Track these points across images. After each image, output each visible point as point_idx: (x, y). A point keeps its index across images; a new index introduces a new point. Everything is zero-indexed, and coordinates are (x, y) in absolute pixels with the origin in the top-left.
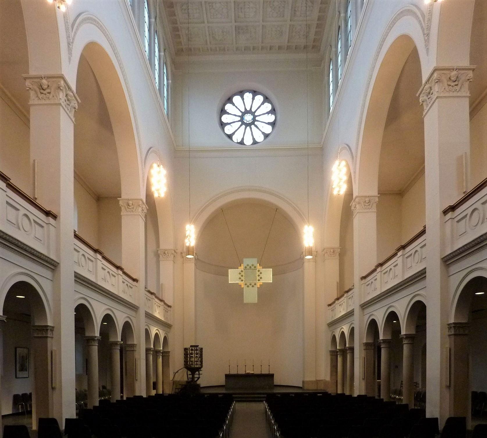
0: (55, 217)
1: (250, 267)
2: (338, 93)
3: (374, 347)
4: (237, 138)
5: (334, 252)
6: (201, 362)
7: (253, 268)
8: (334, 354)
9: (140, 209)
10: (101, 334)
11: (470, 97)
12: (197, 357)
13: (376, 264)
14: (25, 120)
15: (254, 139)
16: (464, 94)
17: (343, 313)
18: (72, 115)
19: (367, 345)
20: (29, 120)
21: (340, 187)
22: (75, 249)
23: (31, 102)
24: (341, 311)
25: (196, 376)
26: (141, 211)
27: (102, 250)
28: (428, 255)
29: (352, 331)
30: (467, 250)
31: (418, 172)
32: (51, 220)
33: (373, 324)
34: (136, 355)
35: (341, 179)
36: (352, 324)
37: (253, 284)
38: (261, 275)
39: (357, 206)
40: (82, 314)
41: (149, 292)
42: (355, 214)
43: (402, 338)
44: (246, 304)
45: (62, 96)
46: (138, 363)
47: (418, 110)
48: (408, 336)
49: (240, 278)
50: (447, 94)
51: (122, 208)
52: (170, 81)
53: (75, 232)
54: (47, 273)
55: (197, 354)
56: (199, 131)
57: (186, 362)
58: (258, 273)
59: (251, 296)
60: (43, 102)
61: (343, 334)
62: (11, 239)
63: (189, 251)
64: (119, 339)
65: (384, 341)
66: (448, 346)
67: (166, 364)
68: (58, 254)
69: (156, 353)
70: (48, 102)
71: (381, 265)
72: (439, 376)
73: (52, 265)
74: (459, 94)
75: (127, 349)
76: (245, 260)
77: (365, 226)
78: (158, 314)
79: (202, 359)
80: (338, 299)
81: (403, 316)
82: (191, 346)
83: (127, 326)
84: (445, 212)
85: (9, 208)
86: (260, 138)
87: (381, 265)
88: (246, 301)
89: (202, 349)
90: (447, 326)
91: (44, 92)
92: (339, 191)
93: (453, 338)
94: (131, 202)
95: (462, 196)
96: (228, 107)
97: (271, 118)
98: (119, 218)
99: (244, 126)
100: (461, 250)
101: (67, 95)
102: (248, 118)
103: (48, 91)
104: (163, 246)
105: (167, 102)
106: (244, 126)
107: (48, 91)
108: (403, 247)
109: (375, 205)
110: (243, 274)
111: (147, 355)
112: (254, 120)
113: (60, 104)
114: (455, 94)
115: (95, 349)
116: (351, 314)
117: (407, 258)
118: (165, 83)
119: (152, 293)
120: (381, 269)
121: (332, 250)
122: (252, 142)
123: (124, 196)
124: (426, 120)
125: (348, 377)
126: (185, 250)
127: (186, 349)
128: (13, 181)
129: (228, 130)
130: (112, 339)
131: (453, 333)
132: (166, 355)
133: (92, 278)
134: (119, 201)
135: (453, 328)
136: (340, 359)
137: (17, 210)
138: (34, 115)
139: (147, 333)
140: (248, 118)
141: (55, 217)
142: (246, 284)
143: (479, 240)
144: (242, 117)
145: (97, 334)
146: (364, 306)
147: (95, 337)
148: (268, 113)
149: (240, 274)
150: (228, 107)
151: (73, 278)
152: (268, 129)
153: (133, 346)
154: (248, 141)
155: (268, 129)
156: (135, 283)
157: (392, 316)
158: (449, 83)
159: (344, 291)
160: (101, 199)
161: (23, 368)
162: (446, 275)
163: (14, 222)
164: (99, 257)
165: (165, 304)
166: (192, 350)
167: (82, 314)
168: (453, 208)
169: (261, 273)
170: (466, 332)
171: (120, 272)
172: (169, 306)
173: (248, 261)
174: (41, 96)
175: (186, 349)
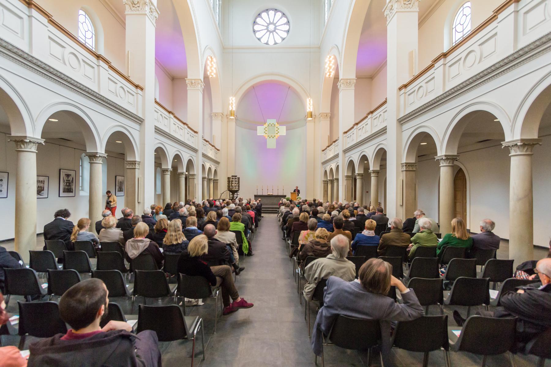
2: (331, 8)
4: (264, 40)
6: (239, 186)
8: (326, 183)
9: (200, 86)
10: (172, 167)
11: (419, 13)
13: (353, 123)
14: (122, 23)
15: (275, 41)
16: (415, 10)
17: (332, 156)
18: (154, 22)
20: (125, 24)
21: (330, 72)
22: (155, 111)
23: (126, 13)
24: (330, 154)
25: (235, 196)
26: (200, 87)
27: (172, 111)
28: (388, 117)
29: (338, 167)
30: (410, 117)
31: (382, 65)
32: (139, 91)
33: (351, 163)
35: (330, 67)
41: (205, 140)
43: (370, 173)
44: (269, 149)
45: (147, 9)
46: (197, 185)
47: (383, 20)
48: (374, 172)
50: (403, 10)
51: (188, 85)
52: (221, 2)
53: (155, 99)
54: (137, 126)
56: (240, 34)
57: (229, 186)
58: (276, 129)
59: (271, 144)
60: (135, 13)
61: (331, 169)
63: (231, 113)
64: (185, 171)
65: (359, 175)
66: (401, 178)
68: (144, 113)
69: (209, 180)
70: (137, 12)
71: (357, 124)
73: (139, 121)
74: (412, 10)
77: (347, 99)
78: (211, 153)
80: (328, 147)
81: (441, 137)
83: (190, 163)
84: (400, 89)
85: (110, 81)
86: (279, 40)
87: (357, 124)
88: (268, 147)
91: (136, 6)
92: (329, 75)
94: (193, 81)
95: (412, 78)
96: (259, 20)
97: (286, 27)
98: (186, 91)
99: (268, 33)
100: (421, 108)
101: (150, 9)
102: (271, 27)
103: (138, 5)
104: (214, 111)
105: (219, 16)
106: (268, 33)
107: (138, 5)
108: (372, 112)
109: (354, 85)
111: (203, 181)
112: (275, 29)
113: (146, 14)
114: (409, 10)
115: (168, 177)
116: (337, 156)
118: (218, 3)
119: (207, 141)
120: (445, 61)
122: (274, 43)
123: (189, 77)
124: (389, 28)
125: (334, 195)
127: (229, 178)
128: (176, 115)
129: (258, 35)
130: (180, 171)
131: (405, 169)
132: (216, 182)
133: (93, 87)
134: (185, 80)
136: (329, 186)
138: (129, 21)
139: (203, 166)
140: (271, 27)
141: (142, 89)
143: (453, 90)
144: (267, 27)
145: (170, 167)
146: (346, 151)
148: (284, 24)
150: (259, 20)
151: (154, 130)
152: (284, 35)
153: (194, 175)
154: (271, 43)
155: (284, 35)
156: (196, 134)
157: (364, 158)
158: (405, 2)
159: (332, 142)
160: (174, 79)
161: (121, 190)
162: (400, 132)
163: (60, 58)
164: (172, 116)
165: (216, 148)
167: (160, 154)
168: (405, 86)
170: (414, 169)
171: (186, 127)
172: (218, 150)
173: (269, 121)
174: (133, 9)
175: (229, 178)
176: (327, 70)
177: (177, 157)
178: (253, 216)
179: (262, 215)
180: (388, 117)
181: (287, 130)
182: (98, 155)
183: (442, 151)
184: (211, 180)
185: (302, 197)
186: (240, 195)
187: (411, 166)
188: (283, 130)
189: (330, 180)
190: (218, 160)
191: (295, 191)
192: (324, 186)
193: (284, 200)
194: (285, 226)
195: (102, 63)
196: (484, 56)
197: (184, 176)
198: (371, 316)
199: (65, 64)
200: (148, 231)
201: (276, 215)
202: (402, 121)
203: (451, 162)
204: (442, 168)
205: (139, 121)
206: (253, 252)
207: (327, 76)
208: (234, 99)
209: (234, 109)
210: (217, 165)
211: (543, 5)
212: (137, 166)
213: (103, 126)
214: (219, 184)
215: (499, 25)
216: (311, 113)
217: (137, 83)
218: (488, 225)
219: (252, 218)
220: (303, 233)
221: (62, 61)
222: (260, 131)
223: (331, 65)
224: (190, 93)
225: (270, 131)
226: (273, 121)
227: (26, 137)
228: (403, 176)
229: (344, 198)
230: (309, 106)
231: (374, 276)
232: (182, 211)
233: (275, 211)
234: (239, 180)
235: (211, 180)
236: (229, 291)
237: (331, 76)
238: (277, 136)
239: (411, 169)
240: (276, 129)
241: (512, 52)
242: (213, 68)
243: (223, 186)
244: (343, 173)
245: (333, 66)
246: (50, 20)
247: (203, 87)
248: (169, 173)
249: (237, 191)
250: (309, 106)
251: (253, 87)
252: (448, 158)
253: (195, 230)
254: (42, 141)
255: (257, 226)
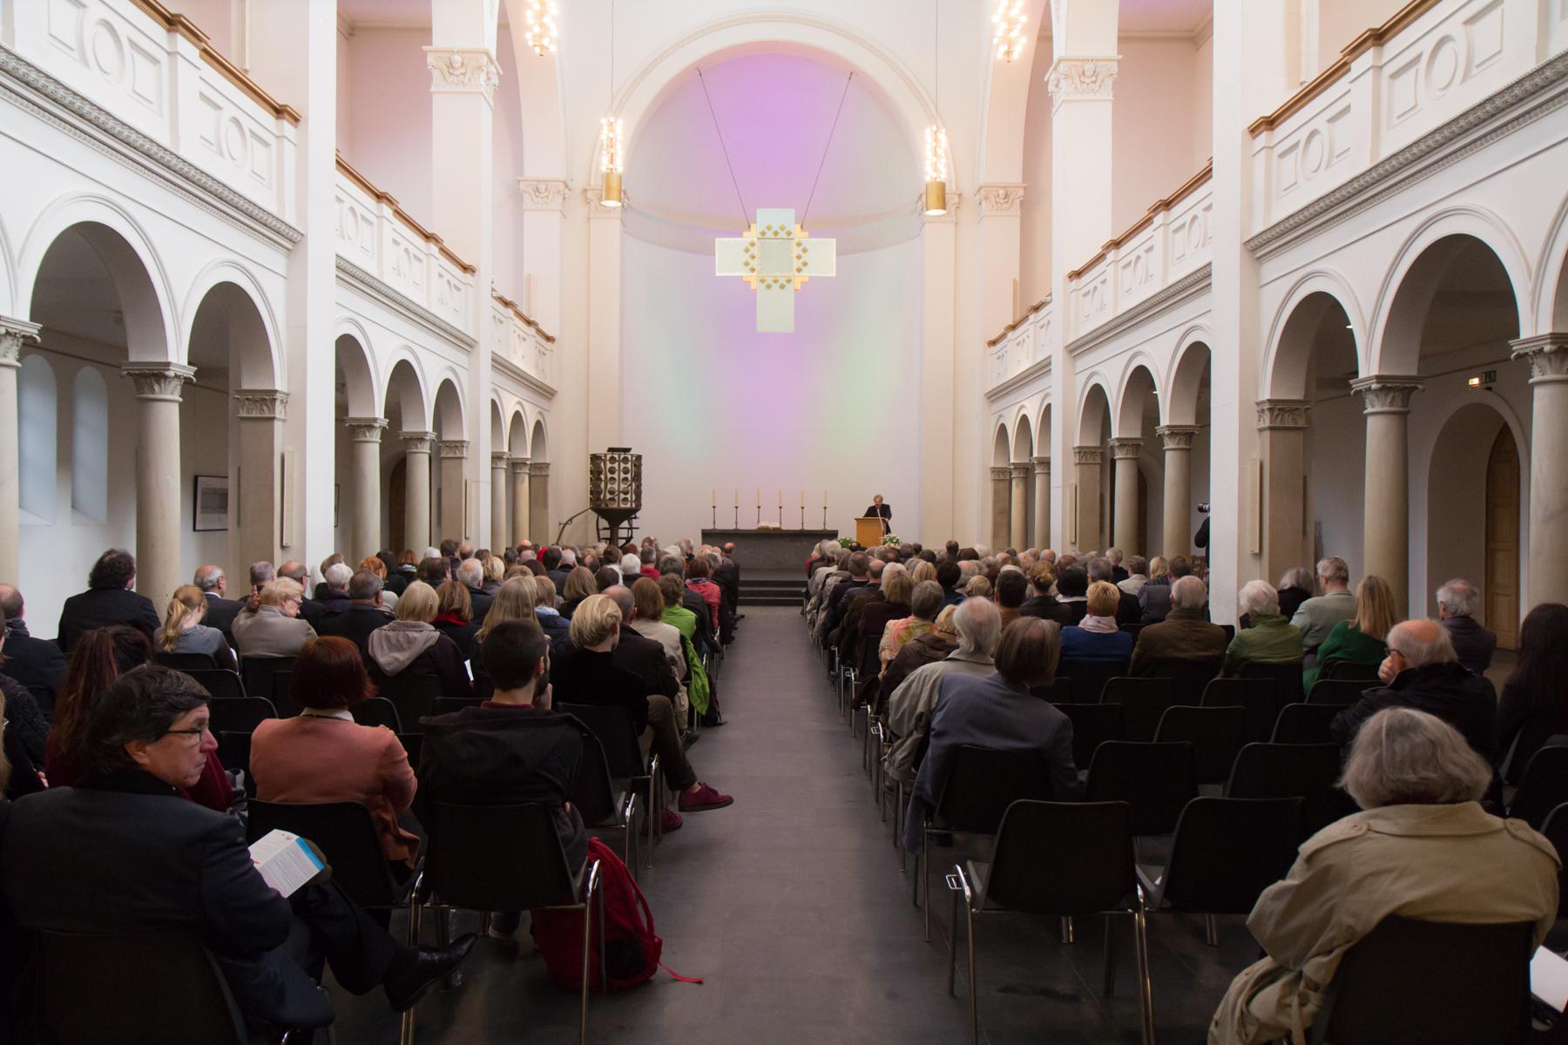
0: (296, 120)
1: (776, 233)
3: (1097, 458)
5: (1006, 196)
6: (638, 494)
7: (782, 234)
8: (1002, 477)
9: (483, 77)
12: (625, 479)
17: (1026, 365)
19: (1082, 451)
21: (1010, 43)
23: (433, 89)
24: (1019, 361)
25: (623, 533)
26: (485, 82)
27: (440, 235)
28: (1211, 233)
32: (287, 126)
33: (1097, 396)
34: (467, 471)
36: (1047, 395)
37: (782, 281)
38: (805, 257)
39: (1063, 83)
40: (349, 354)
42: (1056, 104)
43: (1161, 437)
48: (1175, 431)
49: (747, 264)
51: (435, 73)
54: (274, 258)
55: (626, 471)
57: (595, 493)
58: (797, 251)
59: (775, 313)
61: (1024, 421)
62: (193, 172)
63: (610, 186)
65: (1123, 443)
67: (539, 498)
69: (515, 466)
71: (1117, 244)
72: (1235, 529)
73: (286, 238)
75: (447, 453)
76: (759, 211)
77: (1084, 135)
78: (523, 357)
79: (639, 487)
80: (1013, 327)
82: (611, 450)
83: (447, 391)
87: (1117, 244)
89: (639, 458)
90: (1256, 408)
92: (1008, 53)
93: (1267, 434)
94: (457, 58)
95: (1295, 91)
104: (532, 171)
108: (1167, 205)
109: (1109, 83)
110: (754, 251)
116: (1043, 368)
117: (1176, 231)
119: (507, 304)
120: (1379, 56)
121: (1002, 192)
123: (440, 40)
126: (597, 182)
127: (595, 458)
128: (403, 207)
130: (409, 427)
131: (1267, 424)
132: (539, 472)
133: (154, 127)
134: (424, 55)
135: (1267, 414)
137: (219, 108)
141: (296, 120)
142: (762, 281)
143: (1517, 91)
146: (1078, 349)
147: (375, 420)
149: (747, 250)
151: (334, 271)
153: (459, 445)
156: (468, 277)
157: (1141, 380)
162: (1252, 288)
163: (73, 45)
165: (539, 331)
166: (613, 460)
167: (349, 354)
169: (805, 251)
170: (1301, 423)
171: (434, 249)
172: (549, 339)
173: (767, 217)
175: (595, 458)
176: (1000, 33)
177: (404, 374)
178: (715, 600)
179: (740, 610)
180: (1211, 233)
181: (840, 253)
182: (171, 374)
183: (1369, 365)
184: (524, 471)
185: (904, 530)
186: (645, 527)
187: (1291, 411)
188: (823, 257)
189: (1017, 467)
190: (549, 382)
191: (871, 512)
192: (996, 492)
193: (830, 546)
194: (835, 632)
195: (183, 44)
196: (1477, 61)
197: (425, 448)
198: (1021, 738)
199: (86, 63)
200: (436, 609)
201: (797, 610)
202: (1261, 247)
203: (1398, 400)
204: (1370, 421)
205: (286, 238)
206: (724, 717)
207: (1000, 55)
208: (620, 125)
209: (619, 167)
210: (542, 402)
211: (1494, 15)
212: (279, 411)
213: (183, 265)
214: (551, 482)
215: (1353, 87)
216: (942, 186)
217: (280, 100)
218: (1457, 599)
219: (710, 606)
220: (893, 625)
221: (76, 55)
222: (729, 257)
223: (1014, 12)
224: (438, 104)
225: (770, 257)
226: (783, 217)
227: (168, 364)
228: (1261, 448)
229: (1069, 537)
230: (935, 158)
231: (1019, 651)
232: (466, 569)
233: (789, 595)
234: (637, 477)
235: (524, 471)
236: (678, 774)
237: (1016, 56)
238: (798, 280)
239: (1289, 423)
240: (797, 251)
241: (1530, 65)
242: (546, 20)
243: (570, 487)
244: (1065, 440)
245: (1024, 19)
246: (205, 51)
247: (495, 80)
248: (376, 436)
249: (629, 514)
250: (935, 158)
251: (699, 71)
252: (1387, 385)
253: (552, 617)
254: (33, 330)
255: (727, 638)
